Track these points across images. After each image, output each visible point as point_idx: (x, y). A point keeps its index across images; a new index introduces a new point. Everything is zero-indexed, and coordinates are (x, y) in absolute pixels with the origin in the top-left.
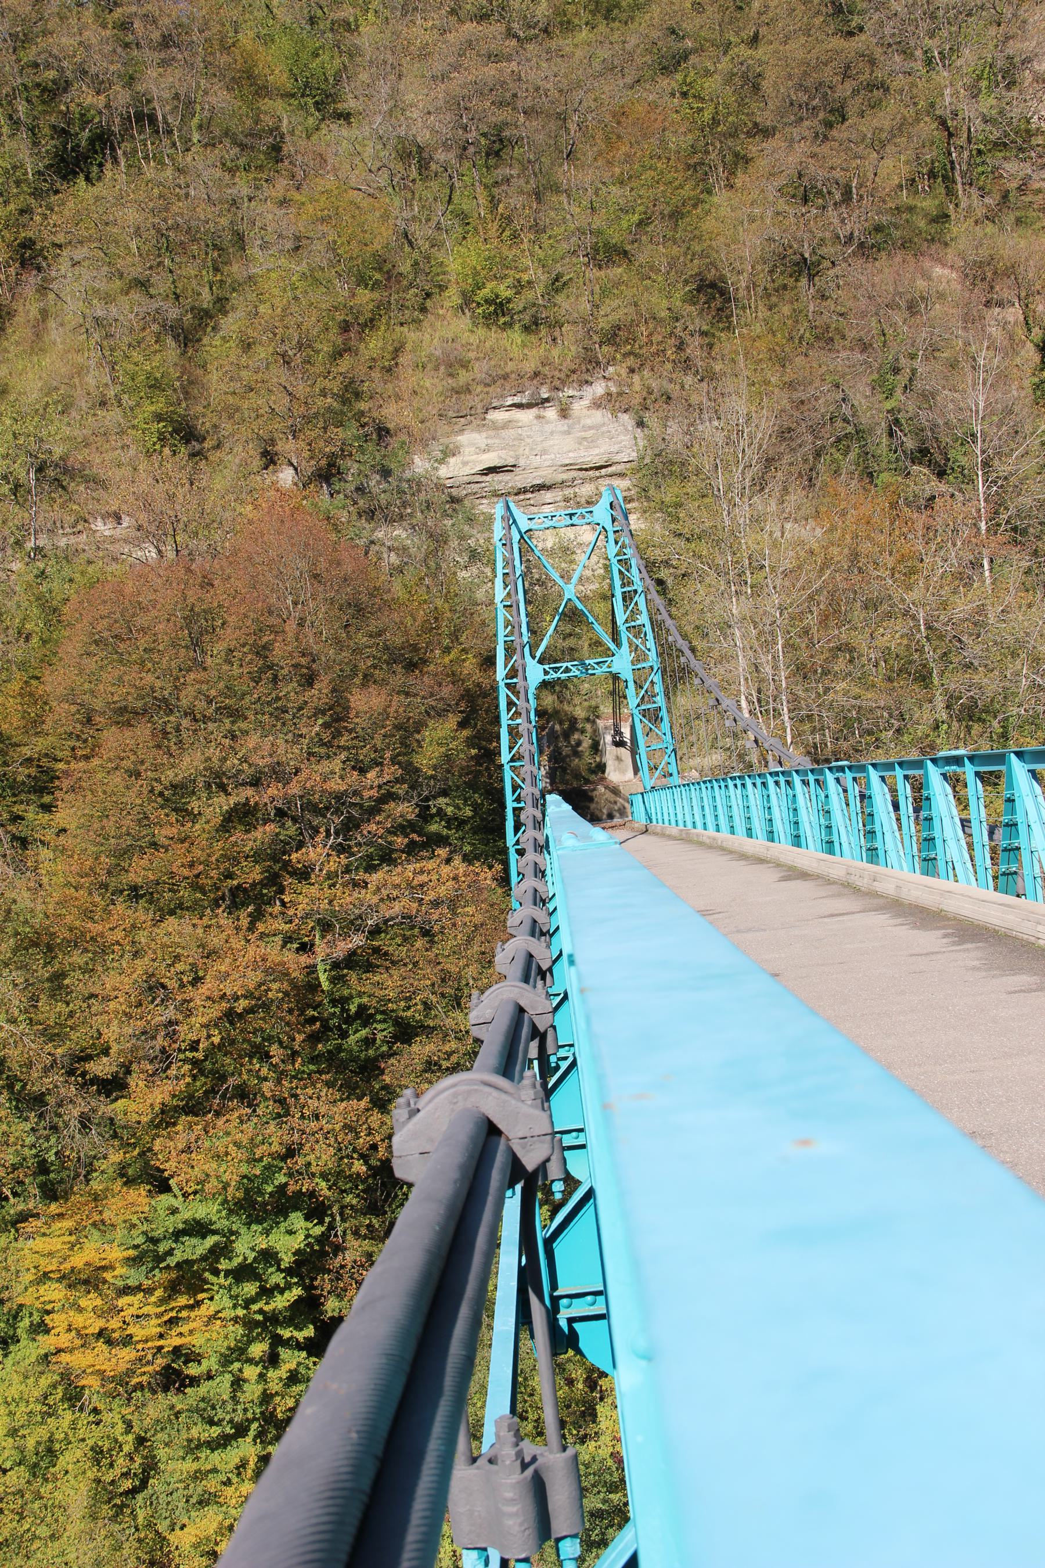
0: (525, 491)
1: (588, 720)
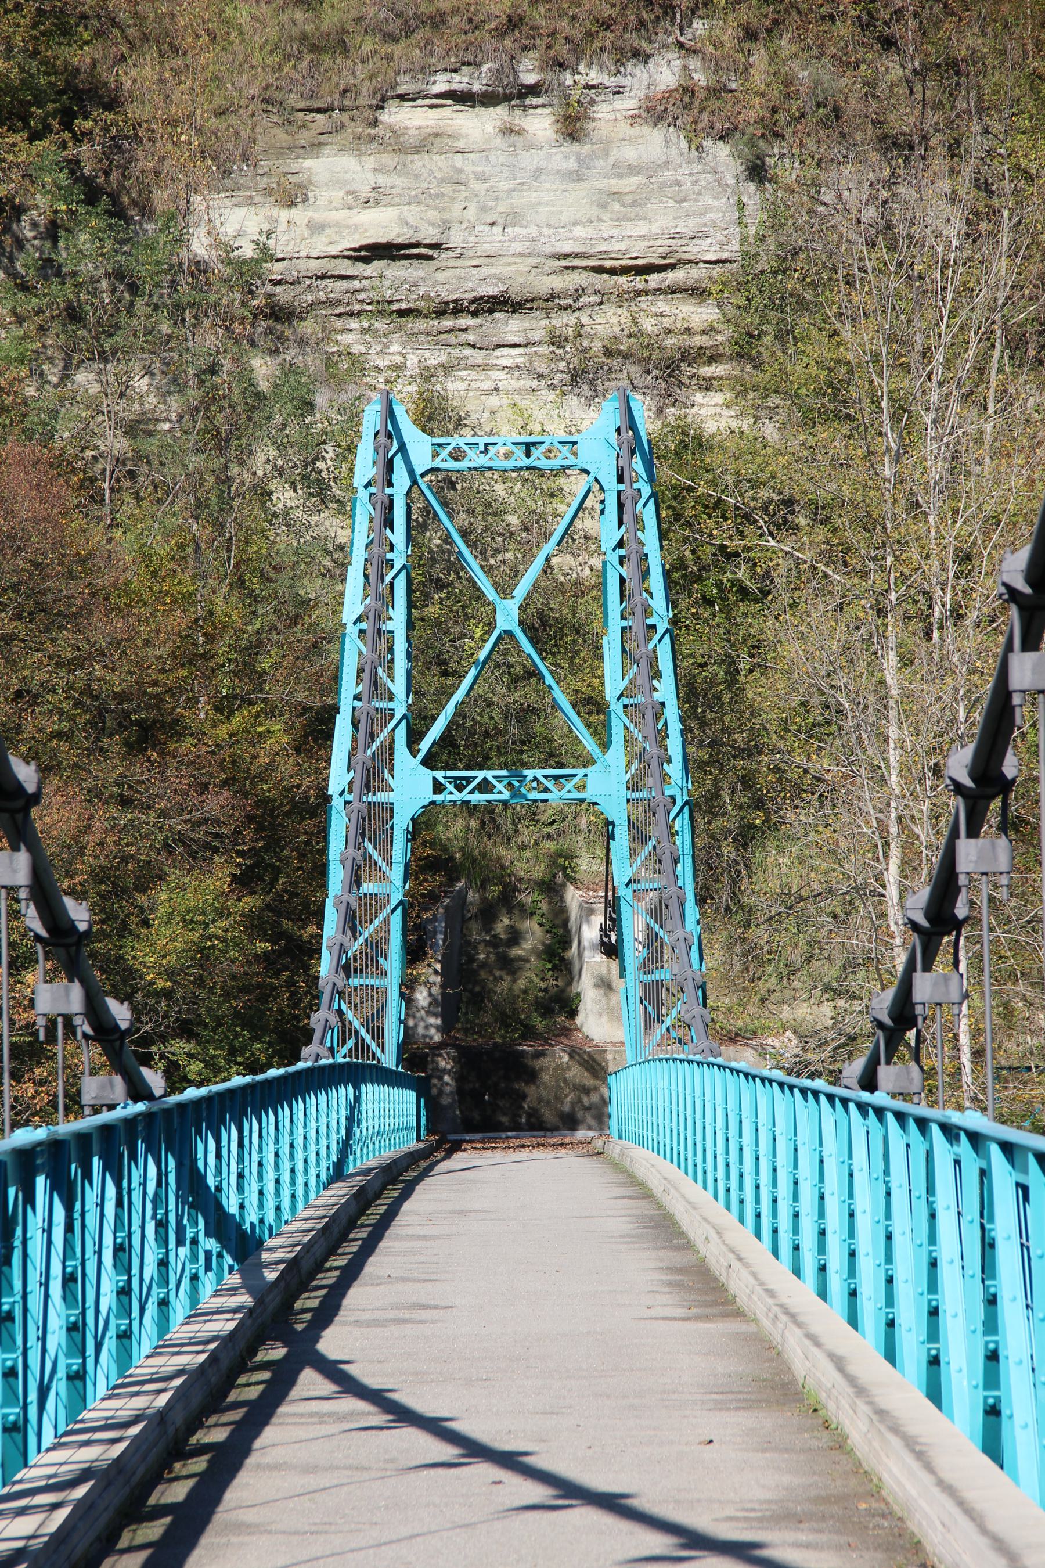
0: (457, 308)
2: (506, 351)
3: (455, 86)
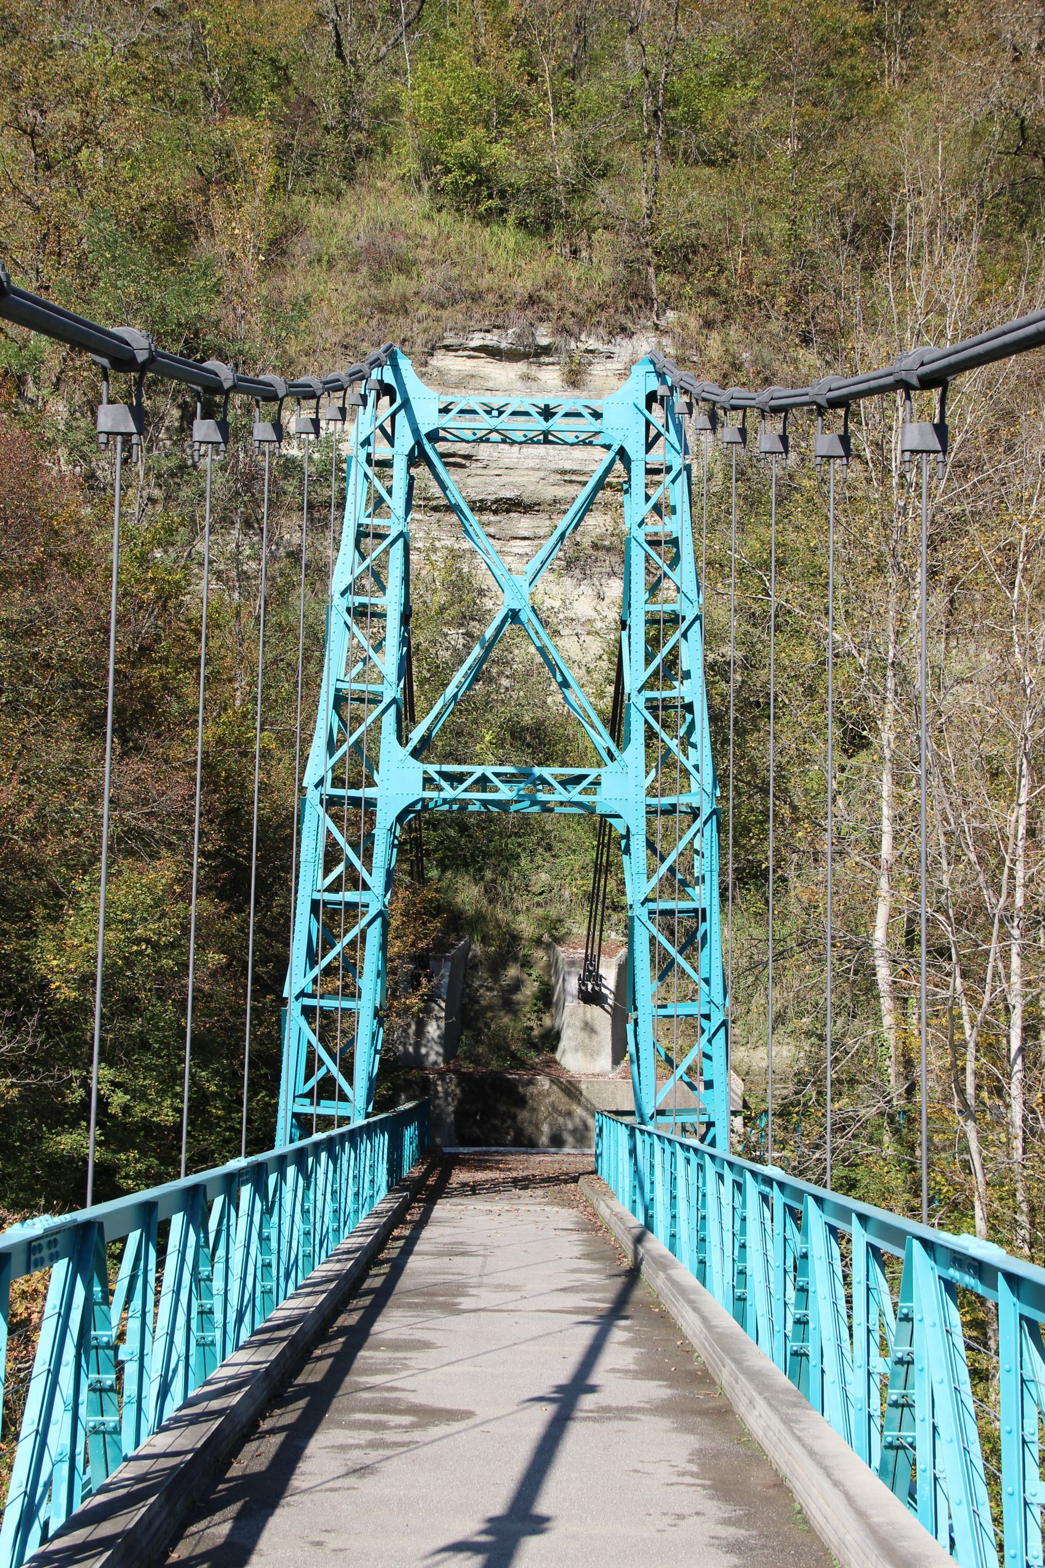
1: (538, 942)
2: (518, 542)
3: (487, 342)
